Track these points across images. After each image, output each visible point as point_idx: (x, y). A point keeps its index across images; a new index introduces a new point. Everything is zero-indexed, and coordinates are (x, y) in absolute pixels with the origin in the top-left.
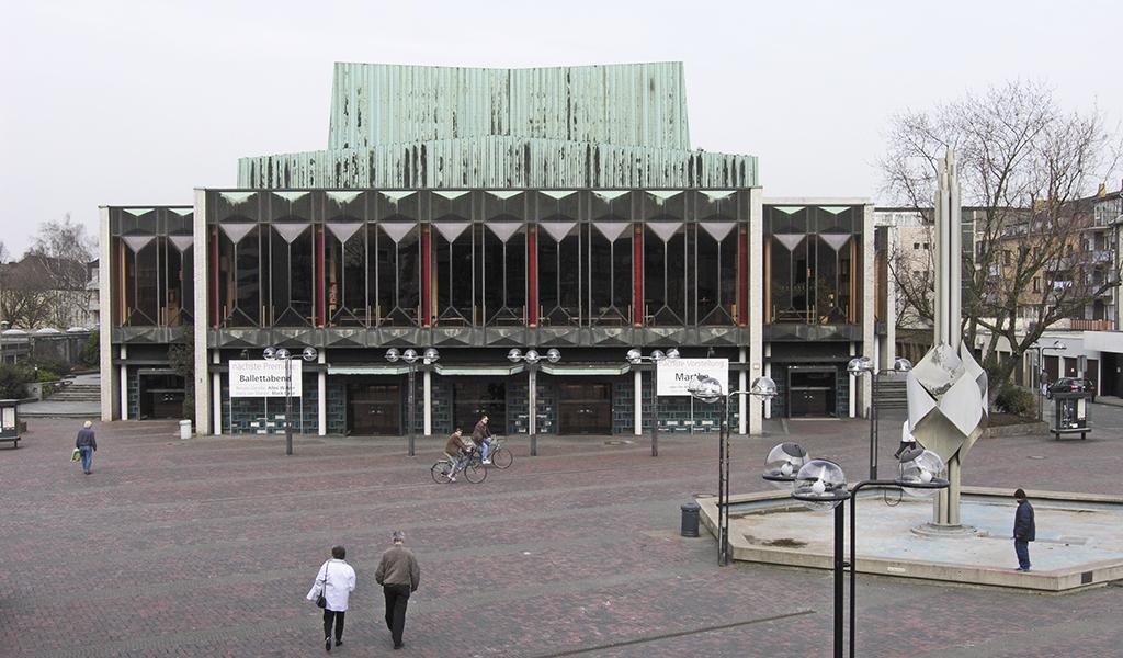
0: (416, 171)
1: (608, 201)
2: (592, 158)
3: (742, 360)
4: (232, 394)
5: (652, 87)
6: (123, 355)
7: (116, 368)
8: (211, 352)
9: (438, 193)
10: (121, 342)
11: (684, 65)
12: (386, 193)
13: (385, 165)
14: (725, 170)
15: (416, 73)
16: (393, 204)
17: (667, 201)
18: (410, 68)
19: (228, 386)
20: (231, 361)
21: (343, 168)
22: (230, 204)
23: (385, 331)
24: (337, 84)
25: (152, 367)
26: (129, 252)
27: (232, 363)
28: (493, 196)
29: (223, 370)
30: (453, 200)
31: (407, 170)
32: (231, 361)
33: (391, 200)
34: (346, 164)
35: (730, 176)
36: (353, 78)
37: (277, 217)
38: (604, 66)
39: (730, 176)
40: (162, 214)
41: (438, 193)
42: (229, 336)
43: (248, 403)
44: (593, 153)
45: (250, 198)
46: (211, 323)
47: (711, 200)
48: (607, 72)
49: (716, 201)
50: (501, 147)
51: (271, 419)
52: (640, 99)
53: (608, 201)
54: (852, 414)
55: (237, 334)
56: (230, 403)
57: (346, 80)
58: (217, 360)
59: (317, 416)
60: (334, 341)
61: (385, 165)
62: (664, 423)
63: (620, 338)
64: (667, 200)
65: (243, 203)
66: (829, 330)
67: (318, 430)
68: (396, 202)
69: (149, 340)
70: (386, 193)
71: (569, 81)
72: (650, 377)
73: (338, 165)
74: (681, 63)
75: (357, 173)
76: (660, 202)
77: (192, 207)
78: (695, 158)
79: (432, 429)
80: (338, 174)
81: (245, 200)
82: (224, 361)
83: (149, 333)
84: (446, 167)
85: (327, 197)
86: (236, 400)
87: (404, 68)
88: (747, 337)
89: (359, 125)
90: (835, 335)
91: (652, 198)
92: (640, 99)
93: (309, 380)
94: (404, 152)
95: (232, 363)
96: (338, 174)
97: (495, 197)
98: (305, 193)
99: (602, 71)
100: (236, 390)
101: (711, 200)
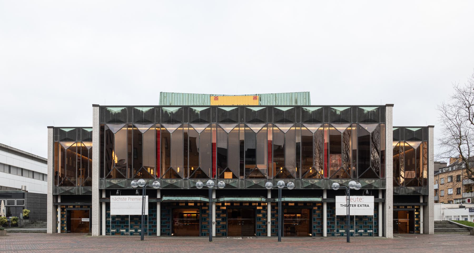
1: (311, 112)
3: (380, 197)
6: (59, 201)
7: (55, 207)
8: (101, 191)
10: (58, 194)
11: (310, 93)
12: (194, 108)
15: (195, 97)
16: (197, 113)
17: (342, 112)
18: (192, 95)
19: (110, 210)
20: (111, 196)
23: (192, 180)
26: (63, 150)
27: (112, 197)
28: (250, 109)
29: (107, 201)
30: (229, 111)
32: (111, 196)
33: (196, 112)
36: (168, 99)
37: (136, 120)
38: (276, 94)
42: (110, 183)
43: (120, 219)
45: (122, 110)
46: (101, 176)
47: (365, 112)
48: (277, 96)
51: (132, 228)
54: (422, 232)
55: (114, 182)
56: (111, 219)
57: (165, 100)
58: (104, 196)
59: (156, 218)
60: (165, 185)
62: (338, 231)
63: (317, 185)
64: (342, 111)
65: (119, 113)
66: (411, 189)
67: (156, 233)
68: (199, 113)
69: (71, 193)
70: (194, 108)
71: (261, 100)
72: (332, 207)
74: (309, 92)
77: (92, 128)
79: (216, 233)
81: (120, 111)
82: (108, 196)
83: (72, 189)
85: (162, 110)
86: (115, 217)
87: (190, 95)
88: (384, 184)
90: (414, 192)
91: (334, 111)
93: (152, 207)
95: (112, 197)
97: (251, 110)
98: (151, 108)
99: (274, 96)
100: (113, 212)
101: (365, 112)
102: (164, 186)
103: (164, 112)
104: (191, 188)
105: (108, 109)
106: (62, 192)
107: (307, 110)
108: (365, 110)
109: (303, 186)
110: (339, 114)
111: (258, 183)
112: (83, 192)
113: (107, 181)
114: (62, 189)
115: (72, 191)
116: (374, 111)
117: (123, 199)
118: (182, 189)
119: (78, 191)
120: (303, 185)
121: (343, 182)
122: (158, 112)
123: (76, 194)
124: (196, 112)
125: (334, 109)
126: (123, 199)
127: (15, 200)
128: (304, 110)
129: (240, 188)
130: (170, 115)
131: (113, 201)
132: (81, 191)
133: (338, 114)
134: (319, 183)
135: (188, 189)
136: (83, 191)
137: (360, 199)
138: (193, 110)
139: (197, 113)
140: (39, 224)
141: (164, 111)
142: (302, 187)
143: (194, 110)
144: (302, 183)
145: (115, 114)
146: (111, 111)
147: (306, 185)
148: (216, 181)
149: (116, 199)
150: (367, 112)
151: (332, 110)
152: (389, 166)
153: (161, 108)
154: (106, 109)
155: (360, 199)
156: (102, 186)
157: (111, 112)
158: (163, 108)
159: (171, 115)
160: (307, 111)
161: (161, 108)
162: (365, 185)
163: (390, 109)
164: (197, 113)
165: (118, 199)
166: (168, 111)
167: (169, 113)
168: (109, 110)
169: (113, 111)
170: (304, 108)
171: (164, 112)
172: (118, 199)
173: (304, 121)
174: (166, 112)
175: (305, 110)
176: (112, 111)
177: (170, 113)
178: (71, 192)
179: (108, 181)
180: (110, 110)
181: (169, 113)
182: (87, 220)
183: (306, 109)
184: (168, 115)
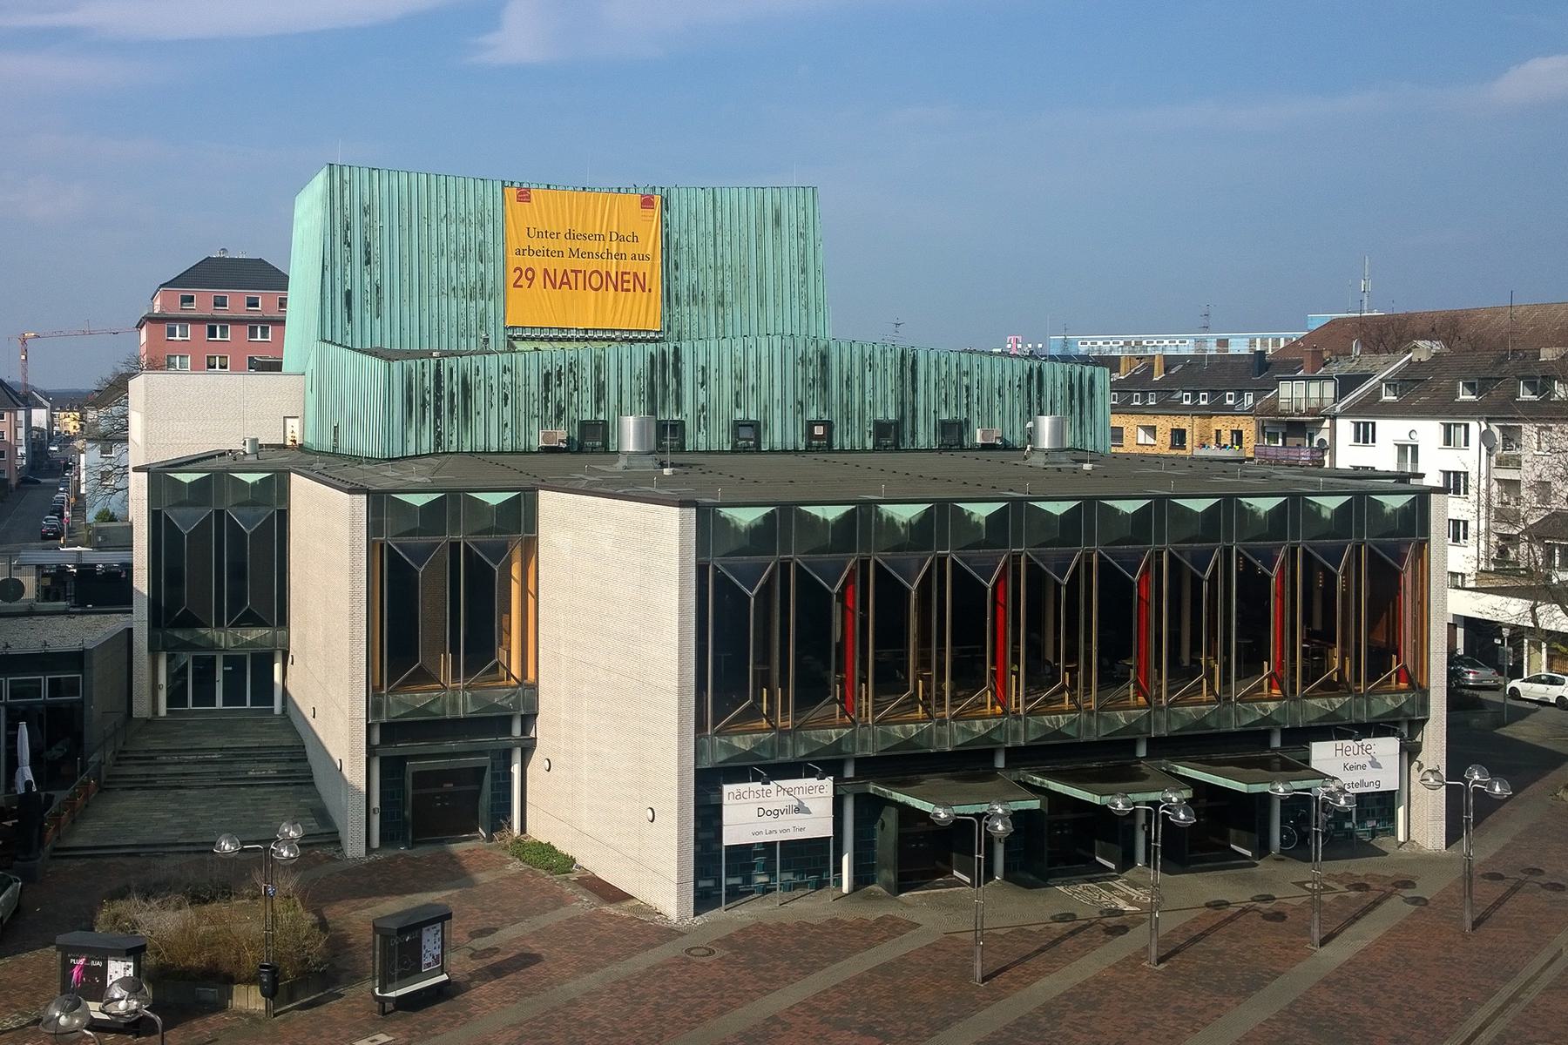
0: (665, 387)
1: (1262, 513)
2: (908, 366)
4: (731, 837)
5: (777, 221)
9: (1036, 504)
12: (965, 506)
13: (620, 375)
14: (1071, 387)
21: (554, 380)
22: (736, 528)
24: (332, 199)
25: (427, 756)
28: (1112, 508)
31: (652, 385)
33: (975, 518)
34: (559, 373)
35: (1076, 395)
39: (1076, 395)
40: (456, 501)
41: (1036, 504)
42: (730, 747)
44: (909, 362)
45: (767, 517)
47: (1388, 509)
49: (1395, 511)
50: (790, 353)
52: (760, 237)
53: (1262, 513)
57: (347, 192)
61: (620, 375)
68: (983, 522)
69: (432, 714)
73: (547, 376)
75: (576, 389)
76: (1326, 514)
78: (1035, 371)
80: (547, 390)
84: (712, 382)
85: (879, 515)
89: (368, 262)
92: (760, 237)
94: (648, 358)
96: (547, 390)
101: (1388, 509)
102: (884, 748)
103: (884, 520)
104: (957, 746)
105: (722, 514)
106: (402, 712)
107: (1253, 507)
108: (1387, 505)
109: (1239, 720)
110: (1329, 517)
111: (1133, 721)
112: (470, 709)
113: (720, 743)
114: (399, 703)
115: (434, 709)
116: (1406, 507)
117: (760, 793)
118: (932, 751)
119: (454, 705)
120: (1239, 720)
121: (1337, 707)
122: (866, 519)
123: (448, 717)
124: (972, 519)
125: (1314, 503)
126: (760, 793)
127: (42, 677)
128: (1245, 508)
129: (1084, 738)
130: (903, 530)
131: (732, 801)
132: (465, 704)
133: (1325, 519)
134: (1279, 710)
135: (949, 749)
136: (469, 705)
137: (1369, 747)
138: (964, 513)
139: (978, 522)
140: (136, 758)
141: (884, 516)
142: (1237, 725)
143: (966, 514)
144: (1237, 714)
145: (746, 531)
146: (735, 522)
147: (1248, 720)
148: (1021, 720)
149: (740, 795)
150: (1393, 510)
151: (1310, 505)
152: (1438, 656)
153: (874, 508)
154: (717, 515)
155: (1369, 747)
156: (704, 757)
157: (733, 525)
158: (882, 506)
159: (906, 532)
160: (1252, 510)
161: (874, 508)
162: (1385, 711)
163: (1441, 502)
164: (978, 522)
165: (746, 795)
166: (897, 518)
167: (900, 525)
168: (727, 516)
169: (739, 519)
170: (1242, 500)
171: (884, 520)
172: (746, 795)
173: (1246, 538)
174: (891, 520)
175: (1247, 506)
176: (738, 521)
177: (903, 523)
178: (432, 712)
179: (723, 741)
180: (729, 517)
181: (900, 525)
182: (702, 884)
183: (1250, 505)
184: (899, 530)
